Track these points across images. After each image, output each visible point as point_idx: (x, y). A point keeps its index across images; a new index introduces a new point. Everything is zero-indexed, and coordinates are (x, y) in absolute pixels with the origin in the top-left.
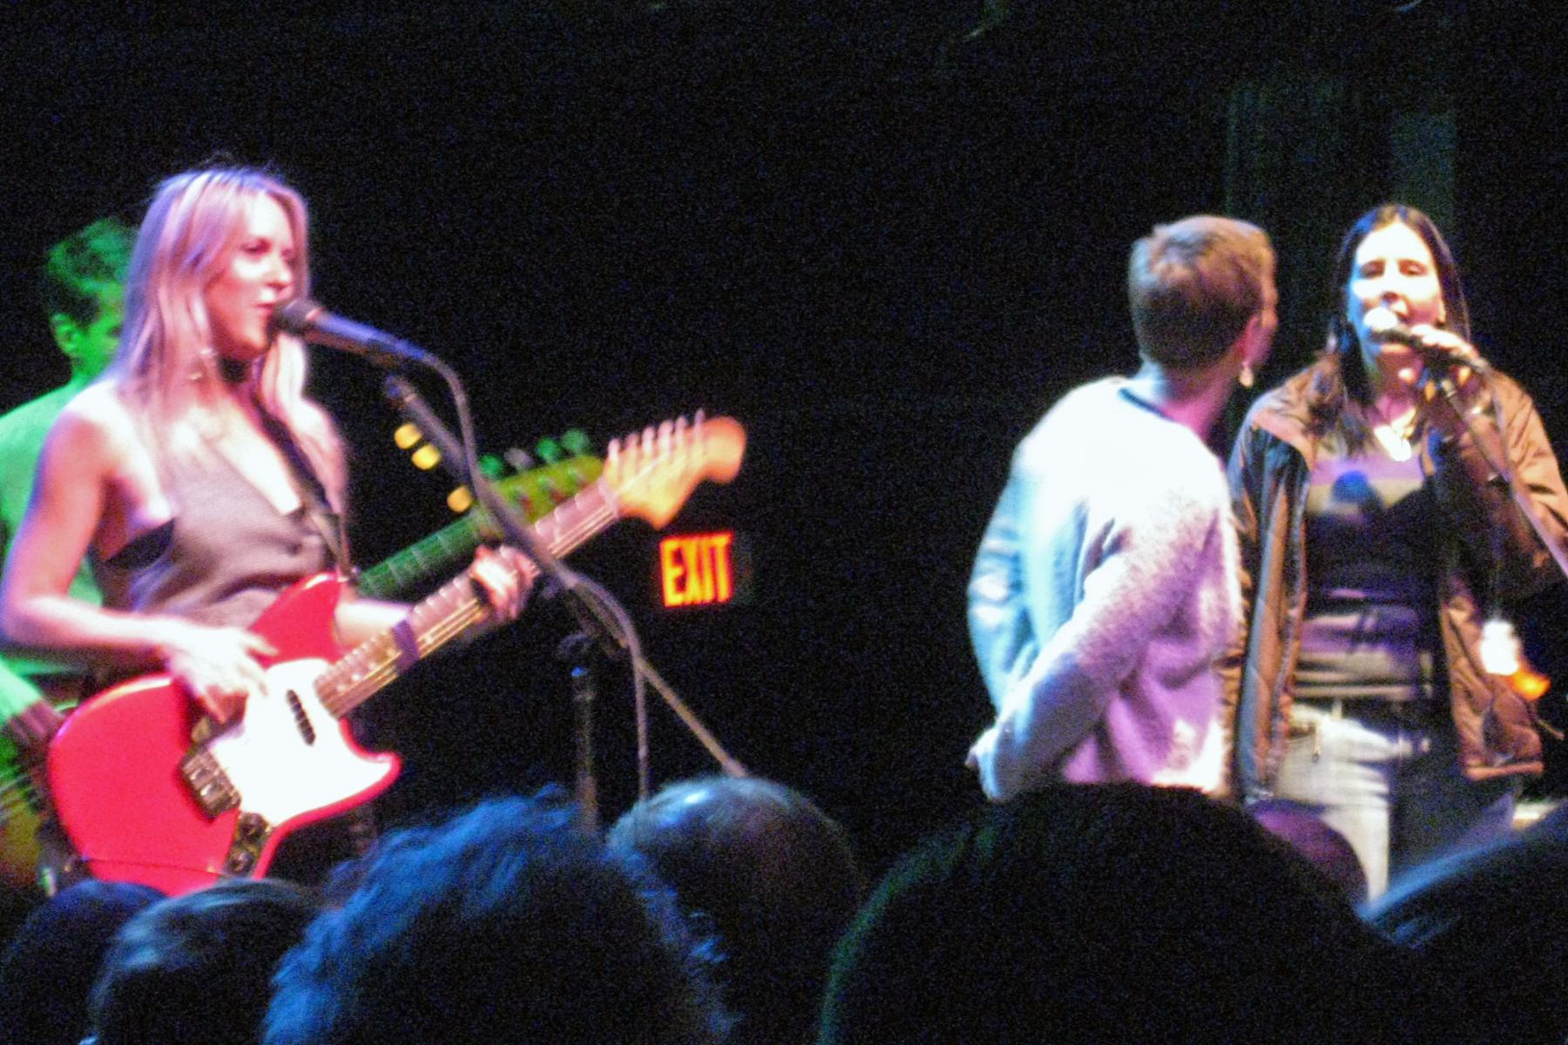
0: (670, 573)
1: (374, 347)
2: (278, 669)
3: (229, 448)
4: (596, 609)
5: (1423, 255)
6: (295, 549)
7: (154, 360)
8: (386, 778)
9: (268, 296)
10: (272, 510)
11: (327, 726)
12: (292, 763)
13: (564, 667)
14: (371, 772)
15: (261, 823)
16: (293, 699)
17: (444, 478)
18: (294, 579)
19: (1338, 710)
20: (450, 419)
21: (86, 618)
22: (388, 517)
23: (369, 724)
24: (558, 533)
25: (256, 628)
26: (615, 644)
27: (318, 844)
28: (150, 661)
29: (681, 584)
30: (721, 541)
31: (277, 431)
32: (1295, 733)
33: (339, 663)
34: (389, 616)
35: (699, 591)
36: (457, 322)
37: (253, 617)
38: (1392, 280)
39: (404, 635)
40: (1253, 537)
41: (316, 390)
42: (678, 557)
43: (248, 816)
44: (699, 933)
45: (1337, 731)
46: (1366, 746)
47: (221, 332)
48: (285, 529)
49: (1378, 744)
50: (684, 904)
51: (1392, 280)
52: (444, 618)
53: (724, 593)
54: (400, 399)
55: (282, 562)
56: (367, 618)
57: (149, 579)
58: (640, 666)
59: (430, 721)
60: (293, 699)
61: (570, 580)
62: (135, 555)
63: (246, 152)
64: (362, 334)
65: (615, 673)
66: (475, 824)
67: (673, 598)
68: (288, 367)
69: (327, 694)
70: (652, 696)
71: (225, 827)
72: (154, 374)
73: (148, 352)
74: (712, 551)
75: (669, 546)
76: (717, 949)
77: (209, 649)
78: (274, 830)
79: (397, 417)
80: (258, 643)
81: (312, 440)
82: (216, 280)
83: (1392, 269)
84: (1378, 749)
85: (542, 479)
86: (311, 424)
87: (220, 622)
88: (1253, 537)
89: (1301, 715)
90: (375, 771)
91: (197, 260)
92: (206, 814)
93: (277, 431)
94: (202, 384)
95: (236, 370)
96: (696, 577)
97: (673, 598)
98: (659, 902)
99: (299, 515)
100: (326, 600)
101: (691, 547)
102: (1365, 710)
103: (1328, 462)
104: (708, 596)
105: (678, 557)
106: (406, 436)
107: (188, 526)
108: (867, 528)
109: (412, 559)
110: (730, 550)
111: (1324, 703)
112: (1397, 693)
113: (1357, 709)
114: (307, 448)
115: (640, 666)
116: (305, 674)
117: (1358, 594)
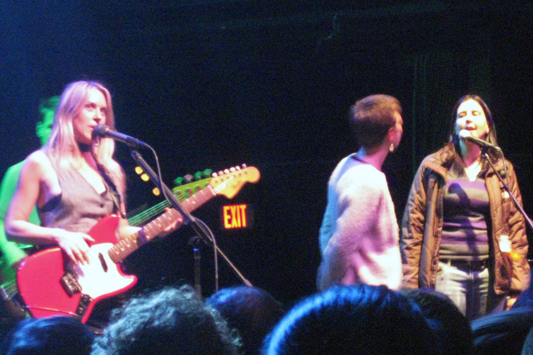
0: (227, 217)
1: (128, 140)
2: (94, 247)
3: (81, 171)
4: (200, 227)
5: (479, 109)
6: (102, 206)
7: (57, 143)
8: (132, 284)
9: (94, 123)
10: (96, 192)
11: (112, 266)
12: (100, 279)
13: (192, 248)
14: (127, 281)
15: (89, 297)
16: (101, 257)
17: (151, 184)
18: (103, 216)
19: (449, 264)
20: (153, 165)
21: (35, 229)
22: (139, 198)
23: (126, 265)
24: (190, 203)
25: (90, 233)
26: (208, 240)
27: (107, 307)
28: (53, 243)
29: (230, 221)
30: (243, 207)
31: (101, 170)
32: (440, 270)
33: (118, 245)
34: (136, 230)
35: (236, 224)
36: (160, 137)
37: (88, 229)
38: (469, 117)
39: (141, 236)
40: (424, 202)
41: (116, 156)
42: (229, 212)
43: (84, 295)
44: (235, 336)
45: (448, 270)
46: (458, 275)
47: (78, 134)
48: (99, 199)
49: (463, 275)
50: (231, 326)
51: (469, 117)
52: (152, 229)
53: (244, 224)
54: (137, 158)
55: (98, 210)
56: (128, 230)
57: (52, 215)
58: (216, 247)
59: (148, 265)
60: (101, 257)
61: (193, 219)
62: (51, 207)
63: (90, 76)
64: (125, 136)
65: (207, 250)
66: (158, 298)
67: (227, 226)
68: (106, 148)
69: (113, 257)
70: (219, 256)
71: (76, 298)
72: (57, 147)
73: (56, 140)
74: (240, 210)
75: (226, 208)
76: (240, 341)
77: (71, 239)
78: (93, 300)
79: (137, 164)
80: (89, 238)
81: (114, 173)
82: (77, 117)
83: (469, 114)
84: (464, 277)
85: (187, 187)
86: (114, 168)
87: (77, 231)
88: (424, 202)
89: (441, 265)
90: (128, 281)
91: (72, 109)
92: (69, 294)
93: (101, 170)
94: (73, 151)
95: (85, 147)
96: (235, 219)
97: (227, 226)
98: (221, 325)
99: (103, 195)
100: (115, 224)
101: (233, 209)
102: (458, 264)
103: (450, 177)
104: (240, 225)
105: (229, 212)
106: (138, 170)
107: (65, 196)
108: (292, 208)
109: (146, 213)
110: (246, 210)
111: (445, 261)
112: (469, 258)
113: (454, 263)
114: (111, 175)
115: (216, 247)
116: (105, 248)
117: (458, 225)
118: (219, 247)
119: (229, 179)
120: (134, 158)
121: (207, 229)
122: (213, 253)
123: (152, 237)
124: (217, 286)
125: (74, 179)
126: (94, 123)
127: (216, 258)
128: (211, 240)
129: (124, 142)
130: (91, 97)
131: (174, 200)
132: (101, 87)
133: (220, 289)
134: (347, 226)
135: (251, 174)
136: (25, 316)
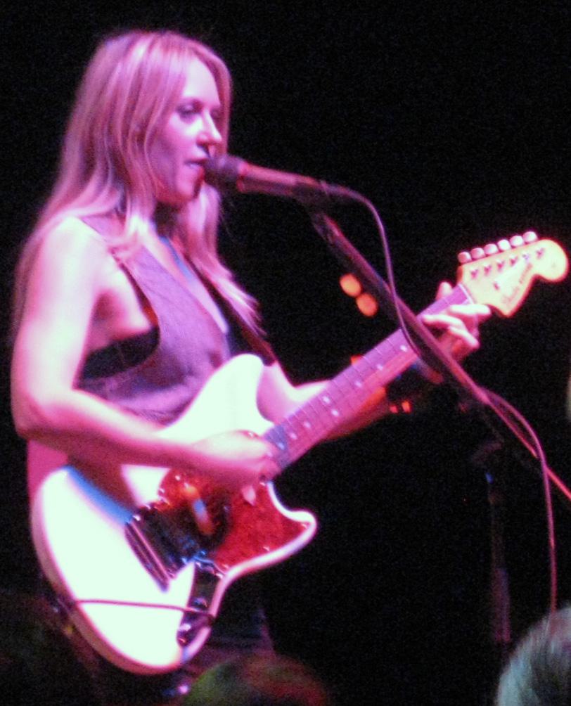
1: (299, 189)
9: (199, 154)
54: (327, 231)
58: (547, 472)
115: (547, 472)
118: (554, 470)
119: (517, 265)
120: (319, 230)
121: (521, 425)
122: (541, 494)
123: (348, 414)
124: (554, 600)
125: (160, 295)
126: (199, 154)
127: (549, 501)
128: (534, 453)
129: (291, 194)
130: (176, 79)
131: (188, 264)
132: (204, 50)
133: (559, 606)
134: (10, 330)
135: (545, 259)
136: (262, 487)
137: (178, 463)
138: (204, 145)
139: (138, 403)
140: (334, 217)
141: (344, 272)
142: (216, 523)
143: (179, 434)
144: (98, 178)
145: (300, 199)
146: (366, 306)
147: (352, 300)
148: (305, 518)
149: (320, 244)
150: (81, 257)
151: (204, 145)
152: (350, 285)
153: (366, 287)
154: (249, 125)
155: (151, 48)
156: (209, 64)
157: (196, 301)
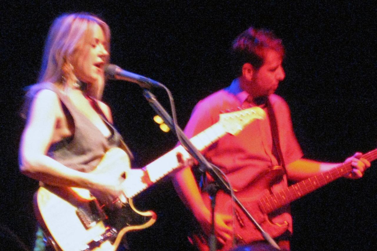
54: (150, 98)
120: (147, 97)
130: (85, 36)
137: (95, 191)
138: (101, 56)
139: (69, 161)
140: (154, 93)
141: (155, 114)
142: (18, 139)
143: (89, 177)
144: (53, 152)
145: (140, 84)
146: (165, 128)
147: (158, 125)
148: (148, 214)
149: (147, 103)
150: (44, 108)
151: (101, 56)
152: (158, 119)
153: (166, 122)
154: (118, 52)
155: (66, 68)
156: (101, 26)
157: (95, 123)
